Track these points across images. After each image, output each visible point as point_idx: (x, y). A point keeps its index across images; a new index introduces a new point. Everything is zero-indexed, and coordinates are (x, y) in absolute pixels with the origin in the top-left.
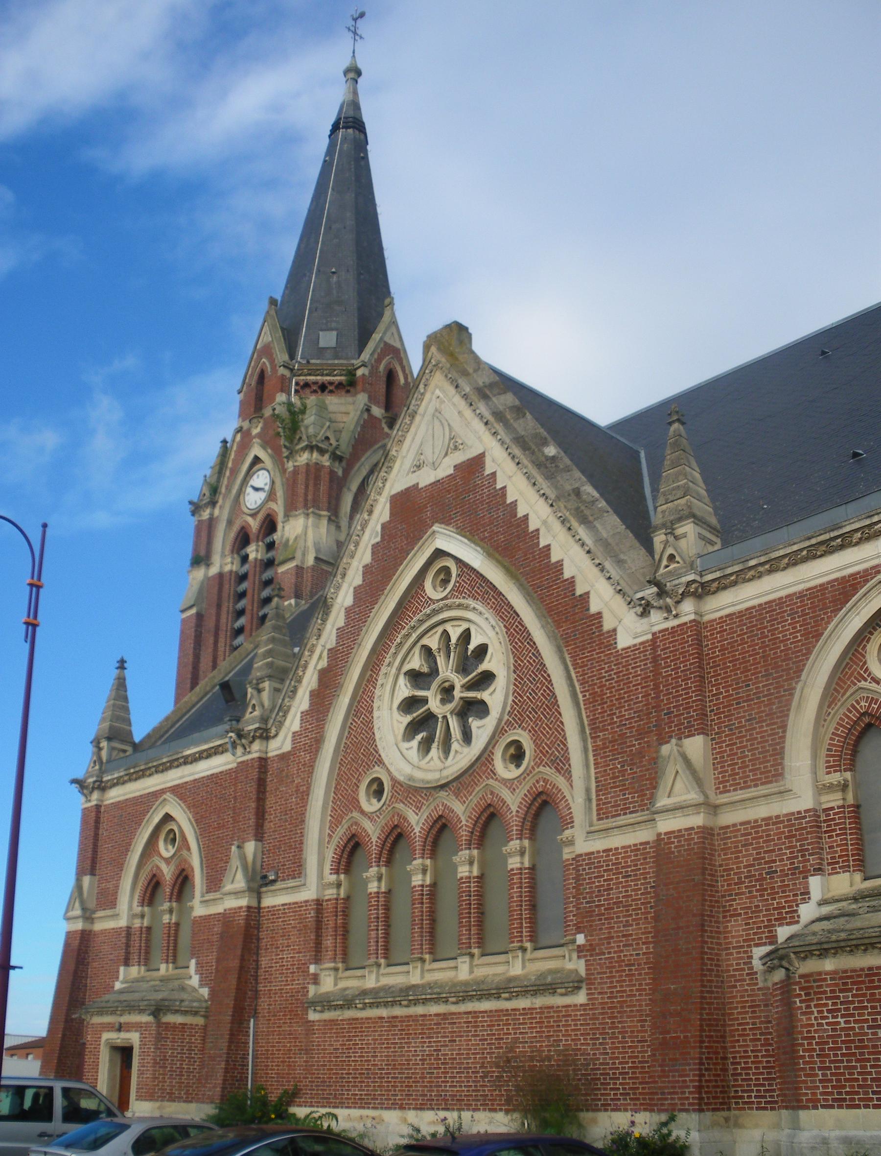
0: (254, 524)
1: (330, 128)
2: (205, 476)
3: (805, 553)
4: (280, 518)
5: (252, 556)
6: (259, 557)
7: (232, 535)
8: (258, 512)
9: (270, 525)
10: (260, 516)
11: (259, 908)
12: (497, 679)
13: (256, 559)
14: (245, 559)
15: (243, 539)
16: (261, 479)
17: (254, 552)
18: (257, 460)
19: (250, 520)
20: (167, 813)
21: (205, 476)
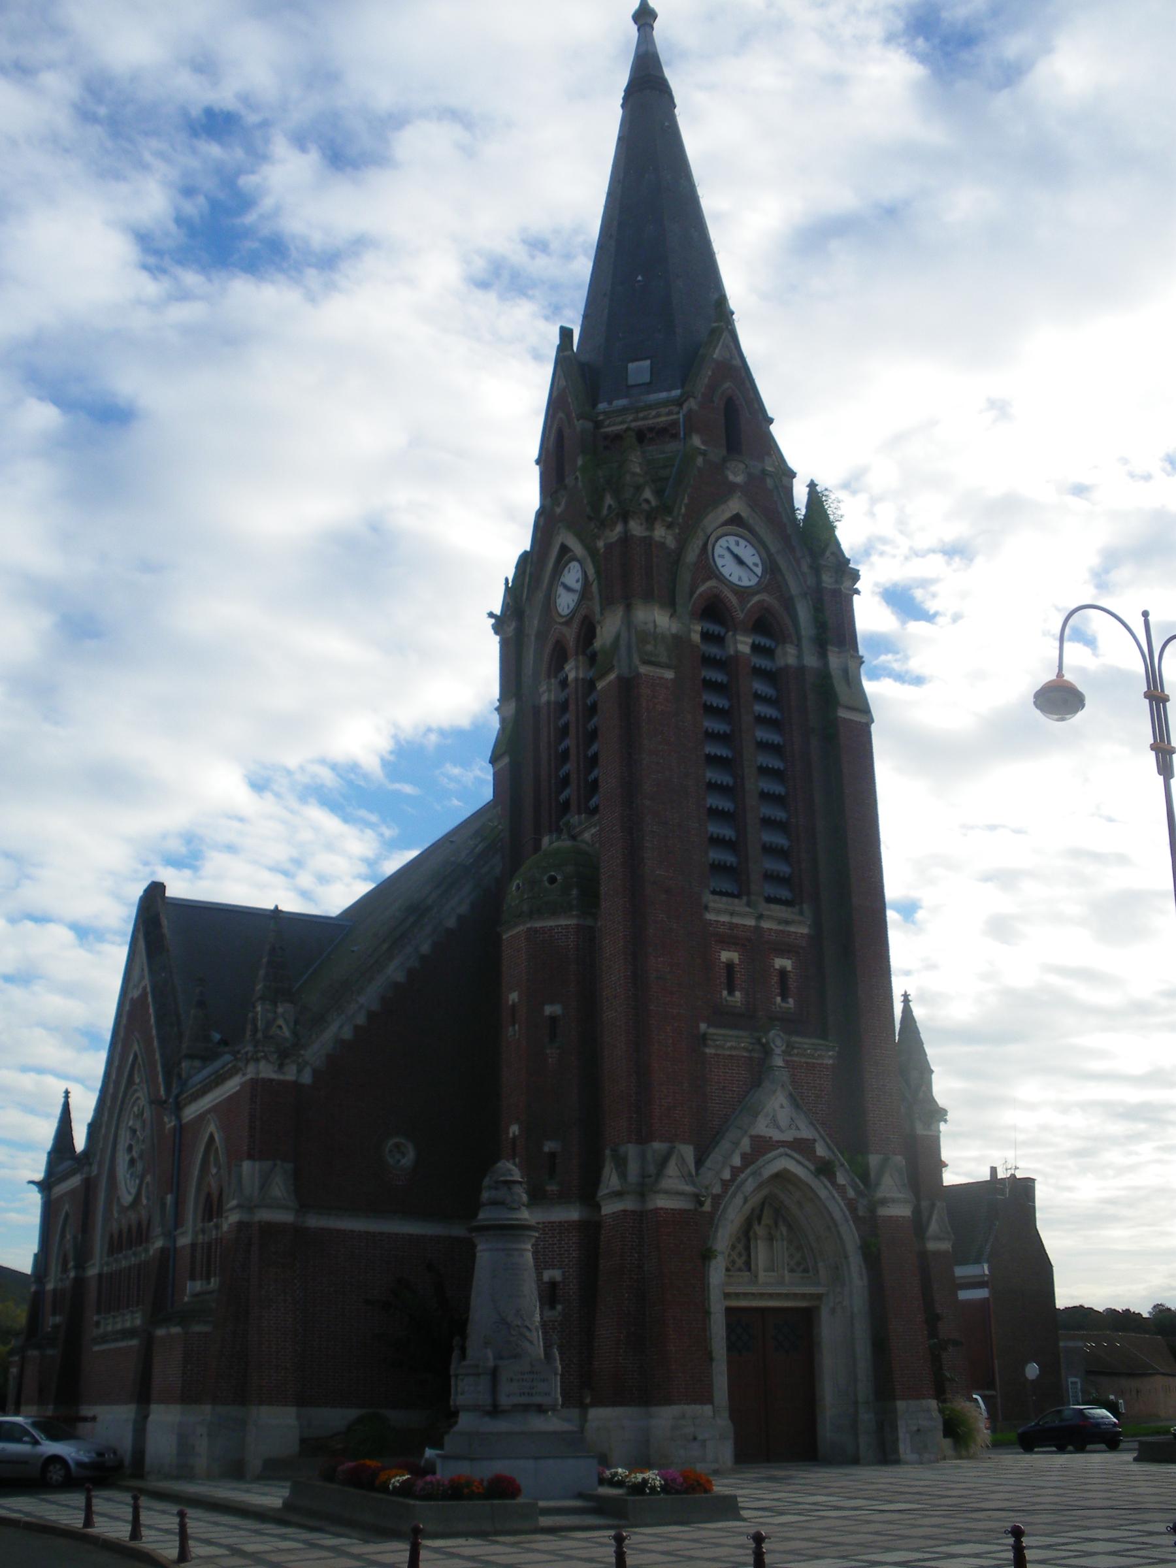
0: (570, 635)
1: (622, 94)
2: (507, 580)
3: (729, 1044)
4: (598, 617)
5: (572, 676)
6: (581, 676)
7: (548, 650)
8: (572, 618)
9: (588, 631)
10: (575, 625)
11: (175, 1248)
12: (1080, 715)
13: (576, 679)
14: (564, 684)
15: (560, 656)
16: (572, 576)
17: (573, 671)
18: (564, 549)
19: (565, 629)
20: (1033, 1180)
21: (507, 580)
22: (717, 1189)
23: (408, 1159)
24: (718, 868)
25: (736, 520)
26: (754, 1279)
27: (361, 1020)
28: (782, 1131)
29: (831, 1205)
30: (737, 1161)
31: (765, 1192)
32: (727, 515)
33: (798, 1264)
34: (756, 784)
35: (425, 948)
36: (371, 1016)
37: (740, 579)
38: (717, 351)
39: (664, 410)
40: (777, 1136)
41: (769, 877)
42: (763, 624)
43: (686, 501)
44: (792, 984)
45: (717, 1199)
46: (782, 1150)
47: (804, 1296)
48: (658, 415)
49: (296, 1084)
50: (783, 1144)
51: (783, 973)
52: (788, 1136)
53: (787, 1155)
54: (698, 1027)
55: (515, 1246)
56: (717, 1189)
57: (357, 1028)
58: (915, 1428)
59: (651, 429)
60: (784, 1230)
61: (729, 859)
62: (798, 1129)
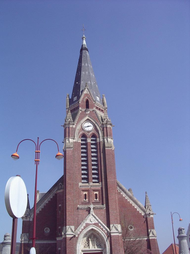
22: (79, 233)
23: (48, 231)
24: (83, 179)
25: (88, 120)
27: (41, 210)
28: (92, 222)
29: (102, 234)
30: (83, 228)
32: (86, 119)
33: (99, 245)
34: (91, 163)
36: (42, 209)
41: (94, 178)
42: (94, 136)
43: (78, 119)
44: (98, 196)
45: (79, 235)
46: (92, 225)
47: (99, 250)
48: (76, 106)
49: (29, 221)
50: (91, 224)
51: (96, 194)
52: (93, 223)
53: (93, 226)
54: (77, 206)
55: (96, 246)
56: (79, 233)
59: (76, 108)
61: (86, 176)
62: (95, 221)
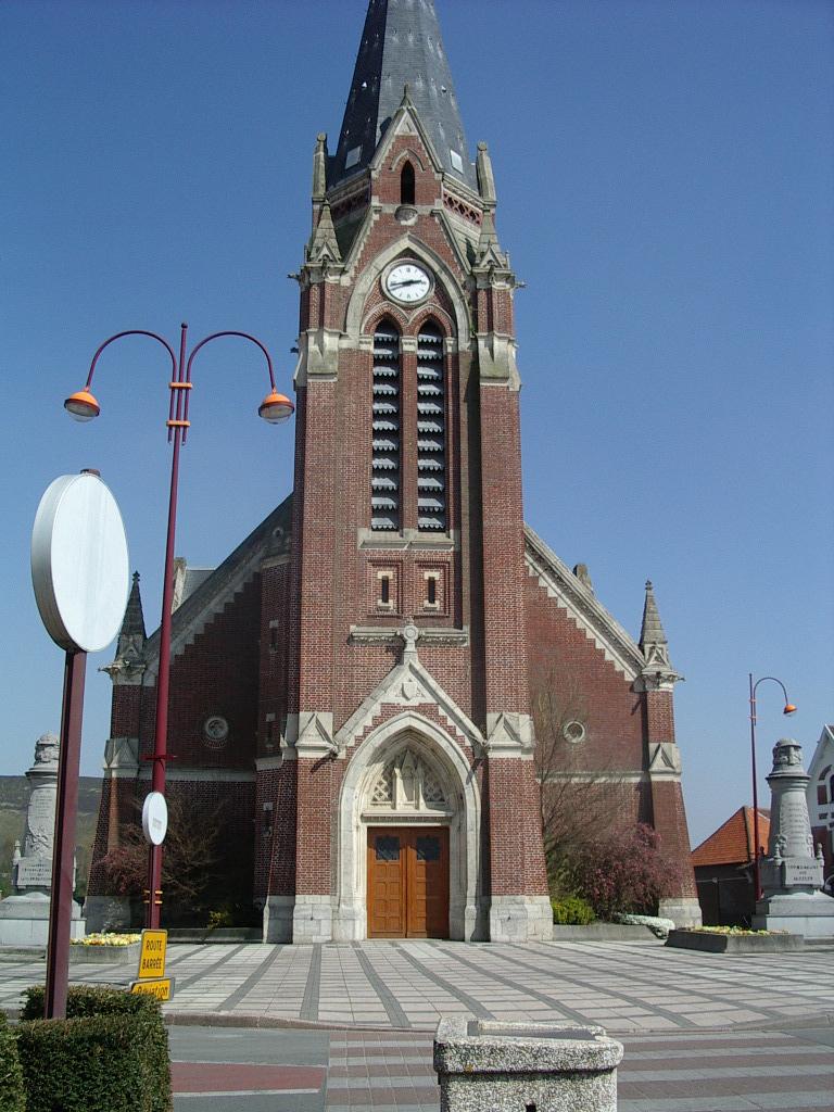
22: (351, 743)
24: (379, 512)
25: (408, 253)
26: (394, 807)
27: (190, 641)
28: (407, 699)
31: (404, 743)
34: (413, 444)
35: (239, 589)
37: (409, 296)
38: (398, 129)
39: (360, 183)
40: (403, 702)
41: (424, 512)
43: (362, 248)
44: (439, 590)
45: (351, 751)
46: (407, 712)
47: (434, 819)
49: (141, 687)
51: (432, 582)
52: (415, 702)
55: (422, 800)
56: (351, 743)
57: (187, 646)
58: (506, 916)
60: (420, 770)
61: (389, 502)
